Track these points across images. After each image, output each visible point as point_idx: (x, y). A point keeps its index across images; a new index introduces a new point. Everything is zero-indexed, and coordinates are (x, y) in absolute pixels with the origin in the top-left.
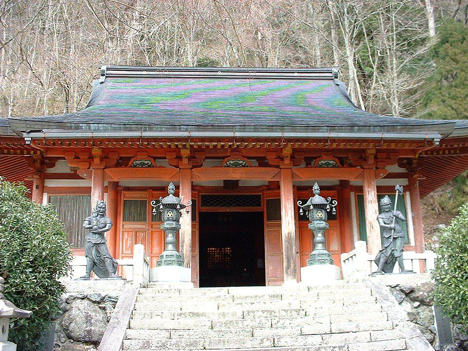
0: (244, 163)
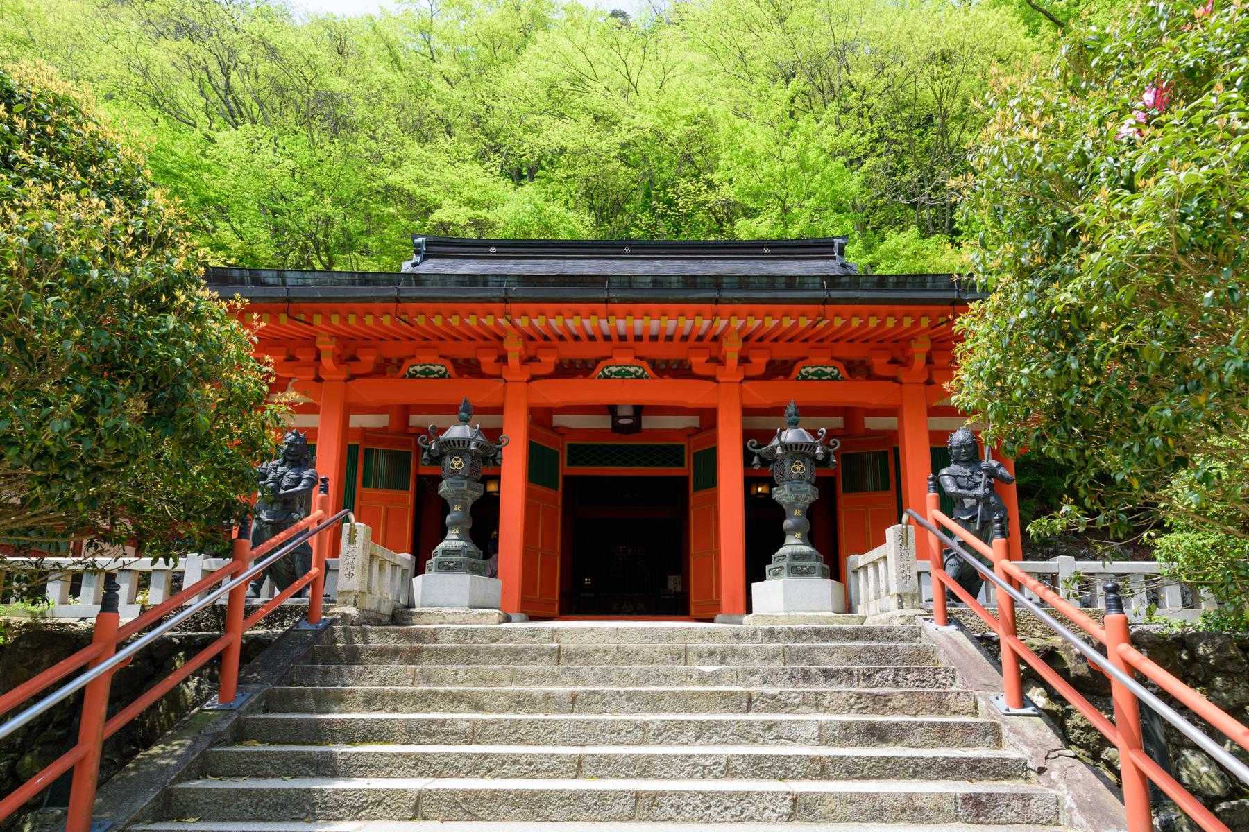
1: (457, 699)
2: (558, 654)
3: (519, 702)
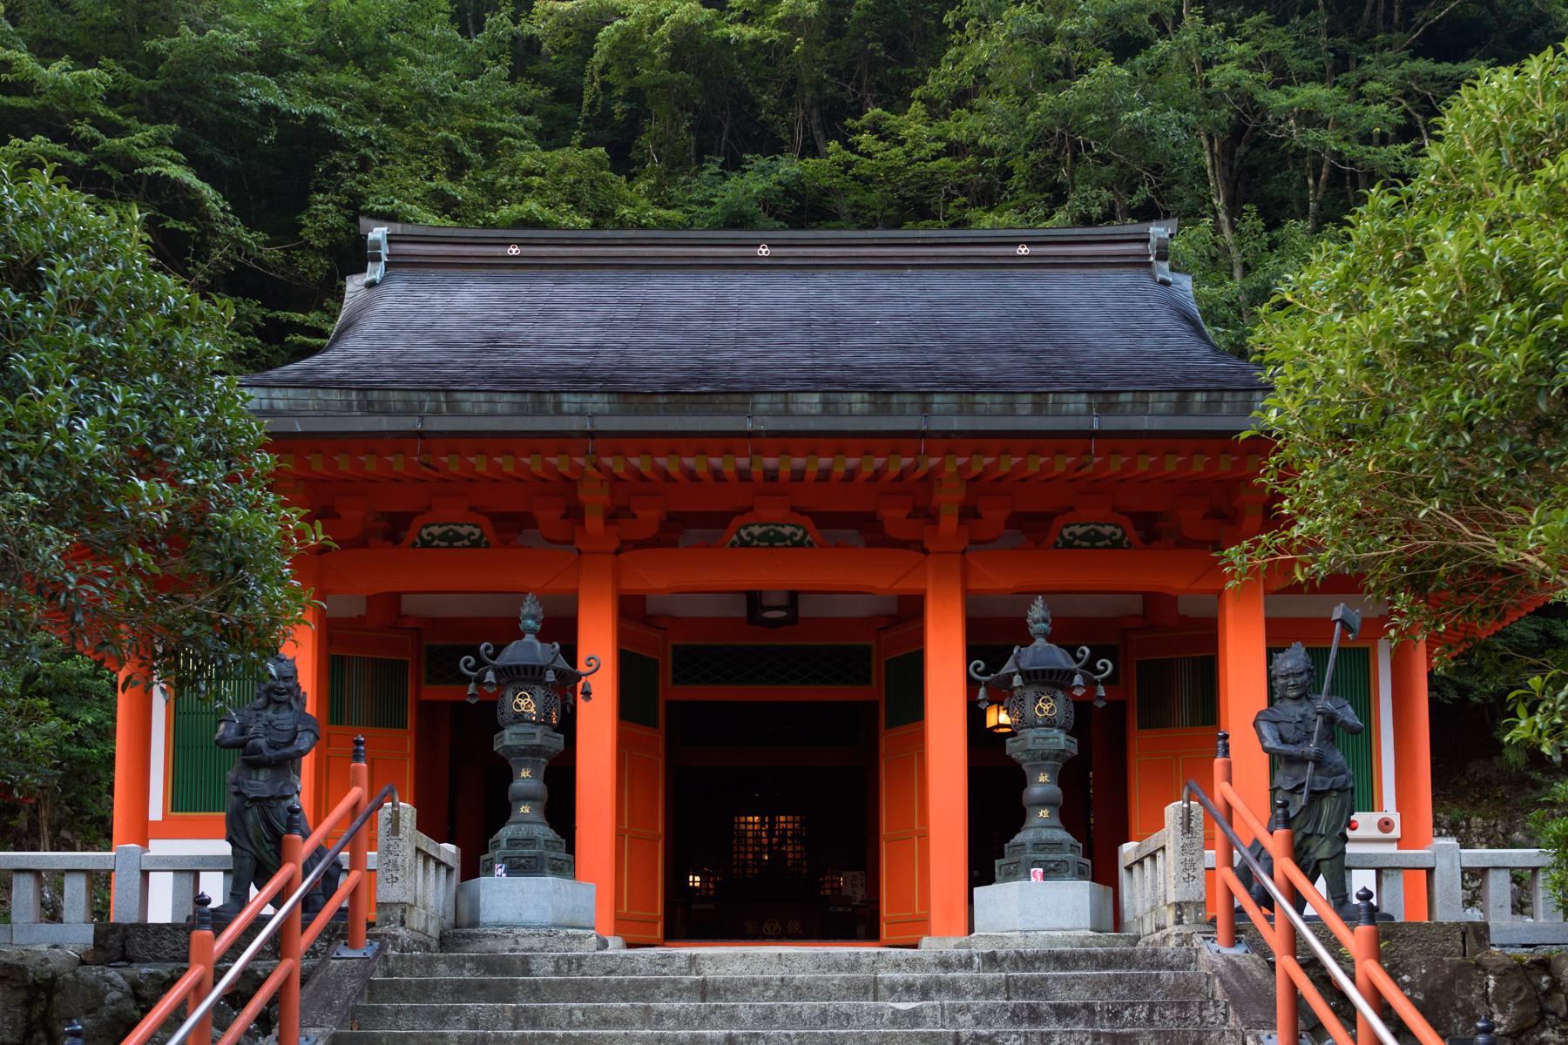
0: (800, 533)
2: (704, 990)
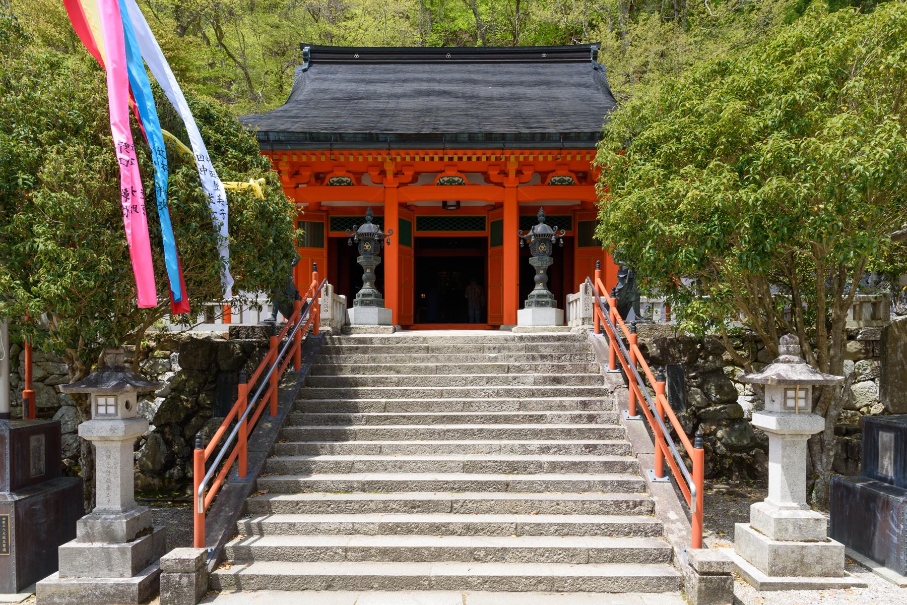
1: (390, 369)
2: (427, 349)
3: (415, 370)
